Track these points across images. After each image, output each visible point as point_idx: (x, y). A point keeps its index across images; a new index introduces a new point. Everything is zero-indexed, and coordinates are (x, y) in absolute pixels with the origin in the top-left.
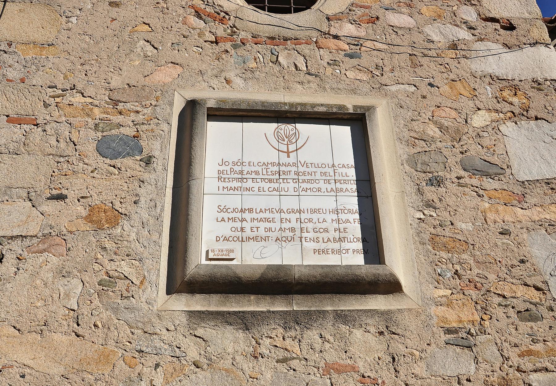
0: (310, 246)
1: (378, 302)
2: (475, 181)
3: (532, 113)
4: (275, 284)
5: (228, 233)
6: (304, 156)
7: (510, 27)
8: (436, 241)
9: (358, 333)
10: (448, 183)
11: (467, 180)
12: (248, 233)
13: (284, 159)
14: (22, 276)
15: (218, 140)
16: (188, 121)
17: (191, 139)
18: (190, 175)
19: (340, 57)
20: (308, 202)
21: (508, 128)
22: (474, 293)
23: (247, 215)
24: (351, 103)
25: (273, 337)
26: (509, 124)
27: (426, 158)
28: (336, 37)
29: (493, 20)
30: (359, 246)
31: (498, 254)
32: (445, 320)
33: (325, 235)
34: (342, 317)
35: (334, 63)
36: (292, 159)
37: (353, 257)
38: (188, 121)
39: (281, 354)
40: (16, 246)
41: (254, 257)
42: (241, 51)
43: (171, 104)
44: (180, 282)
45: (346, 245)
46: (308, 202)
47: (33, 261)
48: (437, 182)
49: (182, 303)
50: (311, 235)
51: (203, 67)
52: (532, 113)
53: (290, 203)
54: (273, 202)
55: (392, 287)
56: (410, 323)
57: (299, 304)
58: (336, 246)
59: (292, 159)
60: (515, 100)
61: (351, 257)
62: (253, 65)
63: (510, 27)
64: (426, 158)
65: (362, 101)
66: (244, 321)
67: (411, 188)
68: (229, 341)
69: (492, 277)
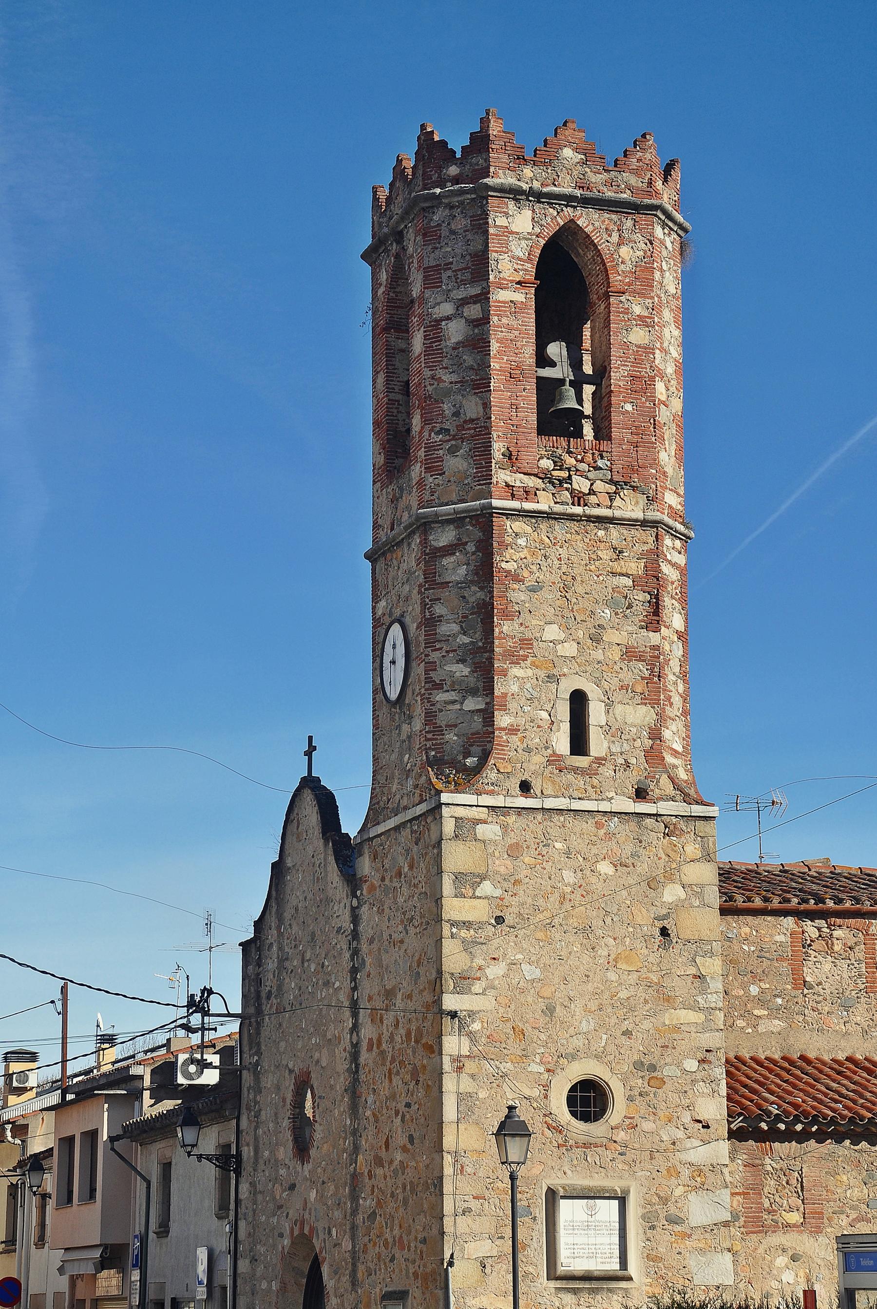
0: (599, 1260)
1: (623, 1284)
2: (670, 1227)
3: (706, 1187)
4: (587, 1277)
5: (569, 1255)
6: (598, 1217)
7: (707, 1127)
8: (651, 1257)
9: (615, 1297)
10: (658, 1229)
11: (666, 1227)
12: (576, 1255)
13: (590, 1219)
14: (494, 1273)
15: (567, 1209)
16: (551, 1210)
17: (554, 1212)
18: (554, 1225)
19: (616, 1155)
20: (600, 1240)
21: (692, 1197)
22: (661, 1281)
23: (575, 1247)
24: (617, 1186)
25: (585, 1297)
26: (693, 1193)
27: (649, 1215)
28: (615, 1142)
29: (699, 1121)
30: (618, 1260)
31: (674, 1264)
32: (648, 1293)
33: (605, 1256)
34: (610, 1290)
35: (613, 1160)
36: (593, 1219)
37: (614, 1265)
38: (551, 1210)
39: (588, 1304)
40: (489, 1260)
41: (580, 1266)
42: (570, 1153)
43: (542, 1188)
44: (552, 1276)
45: (613, 1260)
46: (600, 1240)
47: (497, 1267)
48: (653, 1228)
49: (553, 1284)
50: (600, 1255)
51: (553, 1164)
52: (706, 1187)
53: (592, 1240)
54: (585, 1240)
55: (630, 1279)
56: (634, 1293)
57: (594, 1285)
58: (609, 1260)
59: (593, 1219)
60: (698, 1179)
61: (614, 1265)
62: (575, 1162)
63: (707, 1127)
64: (649, 1215)
65: (623, 1183)
66: (575, 1291)
67: (641, 1231)
68: (569, 1298)
69: (670, 1274)
